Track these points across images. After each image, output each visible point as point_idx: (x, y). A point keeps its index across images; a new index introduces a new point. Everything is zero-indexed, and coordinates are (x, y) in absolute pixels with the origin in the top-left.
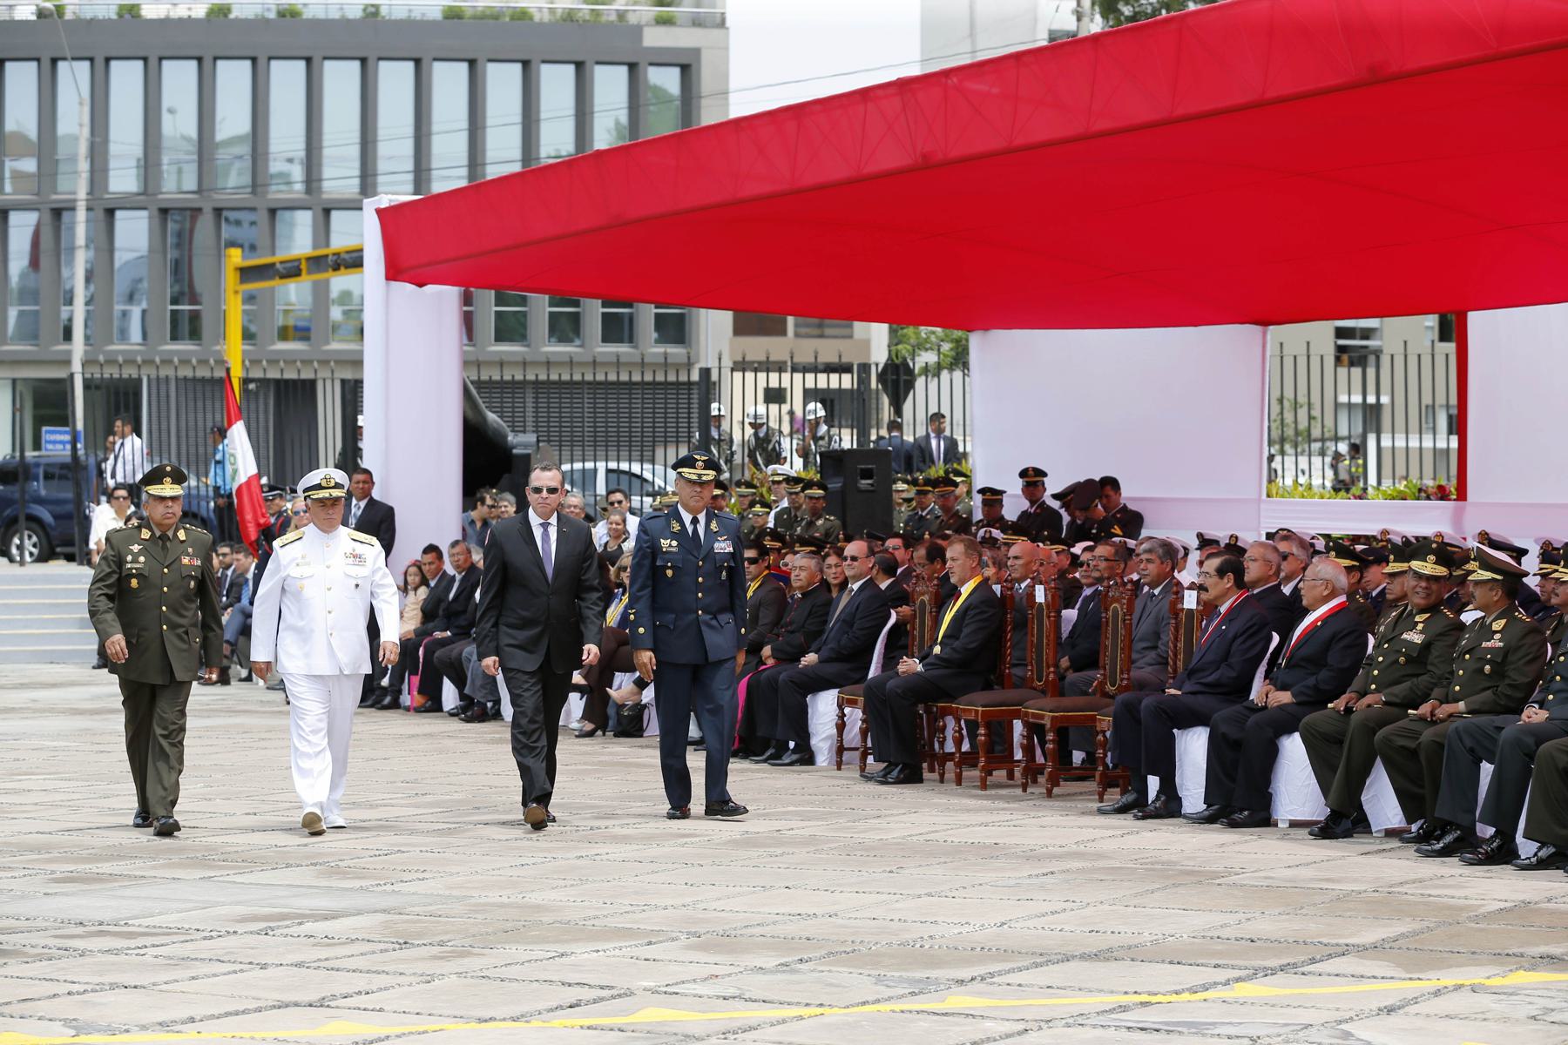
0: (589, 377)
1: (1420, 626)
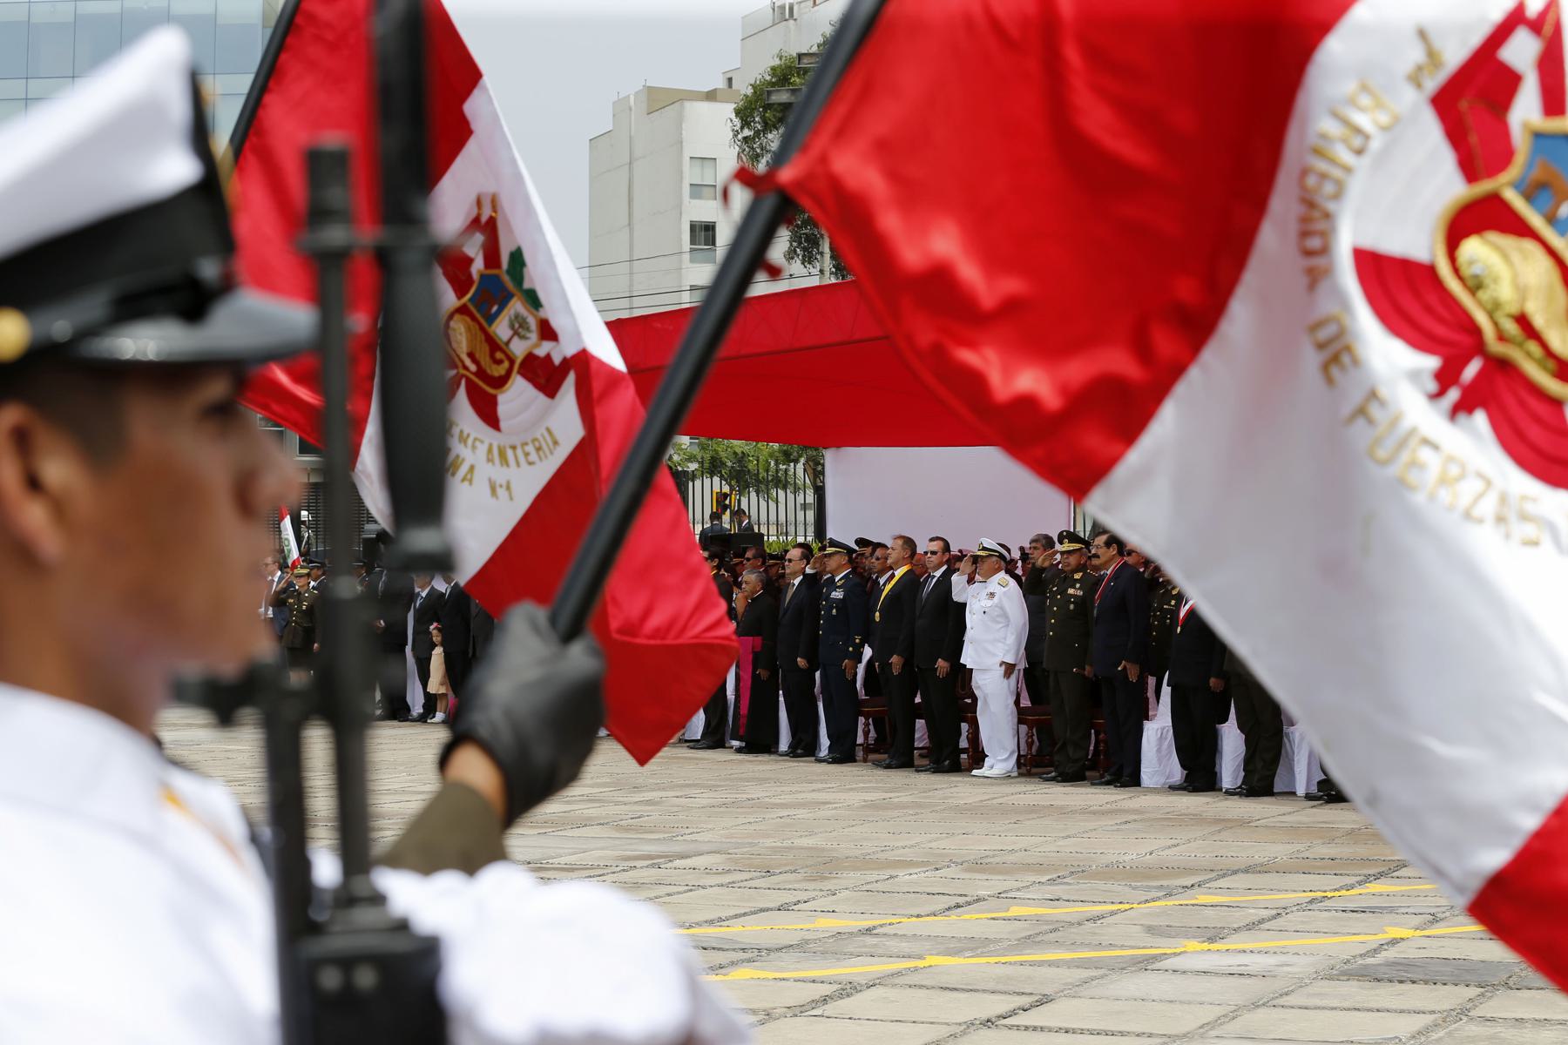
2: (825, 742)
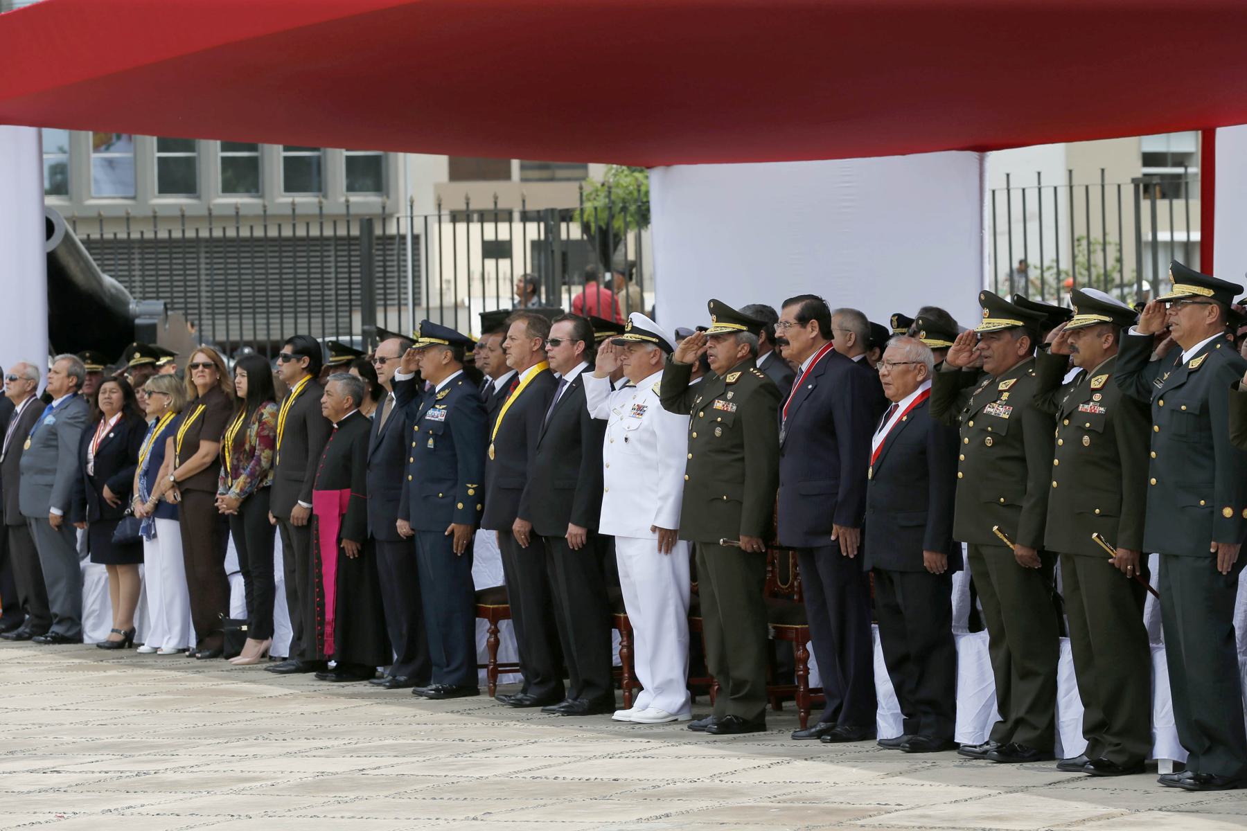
0: (204, 234)
1: (1005, 396)
2: (1166, 744)
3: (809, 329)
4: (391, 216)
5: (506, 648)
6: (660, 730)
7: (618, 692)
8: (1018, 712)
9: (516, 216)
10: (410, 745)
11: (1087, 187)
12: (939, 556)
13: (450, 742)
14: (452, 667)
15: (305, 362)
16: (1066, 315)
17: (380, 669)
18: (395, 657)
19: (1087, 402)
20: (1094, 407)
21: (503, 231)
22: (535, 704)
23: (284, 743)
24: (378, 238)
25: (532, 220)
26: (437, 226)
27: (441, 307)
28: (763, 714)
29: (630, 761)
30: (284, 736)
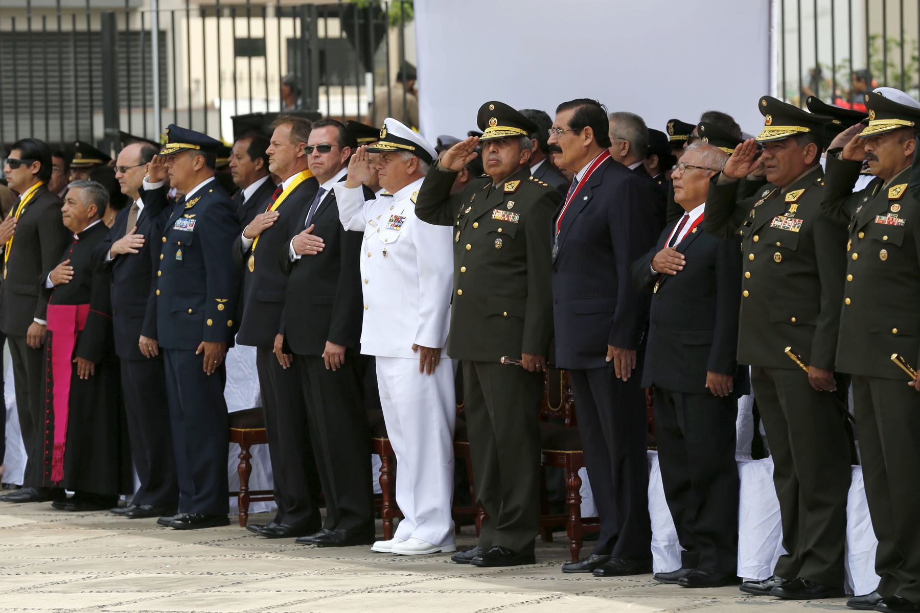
1: (793, 208)
3: (583, 136)
4: (134, 10)
5: (258, 475)
6: (422, 562)
7: (378, 522)
8: (807, 544)
9: (270, 11)
10: (154, 579)
11: (173, 13)
12: (725, 378)
13: (197, 575)
14: (203, 493)
15: (36, 167)
16: (860, 119)
17: (123, 498)
18: (138, 485)
19: (884, 214)
20: (893, 218)
21: (256, 28)
22: (288, 534)
23: (18, 578)
24: (121, 33)
25: (210, 15)
26: (184, 21)
27: (190, 110)
28: (532, 544)
29: (390, 595)
30: (18, 571)
